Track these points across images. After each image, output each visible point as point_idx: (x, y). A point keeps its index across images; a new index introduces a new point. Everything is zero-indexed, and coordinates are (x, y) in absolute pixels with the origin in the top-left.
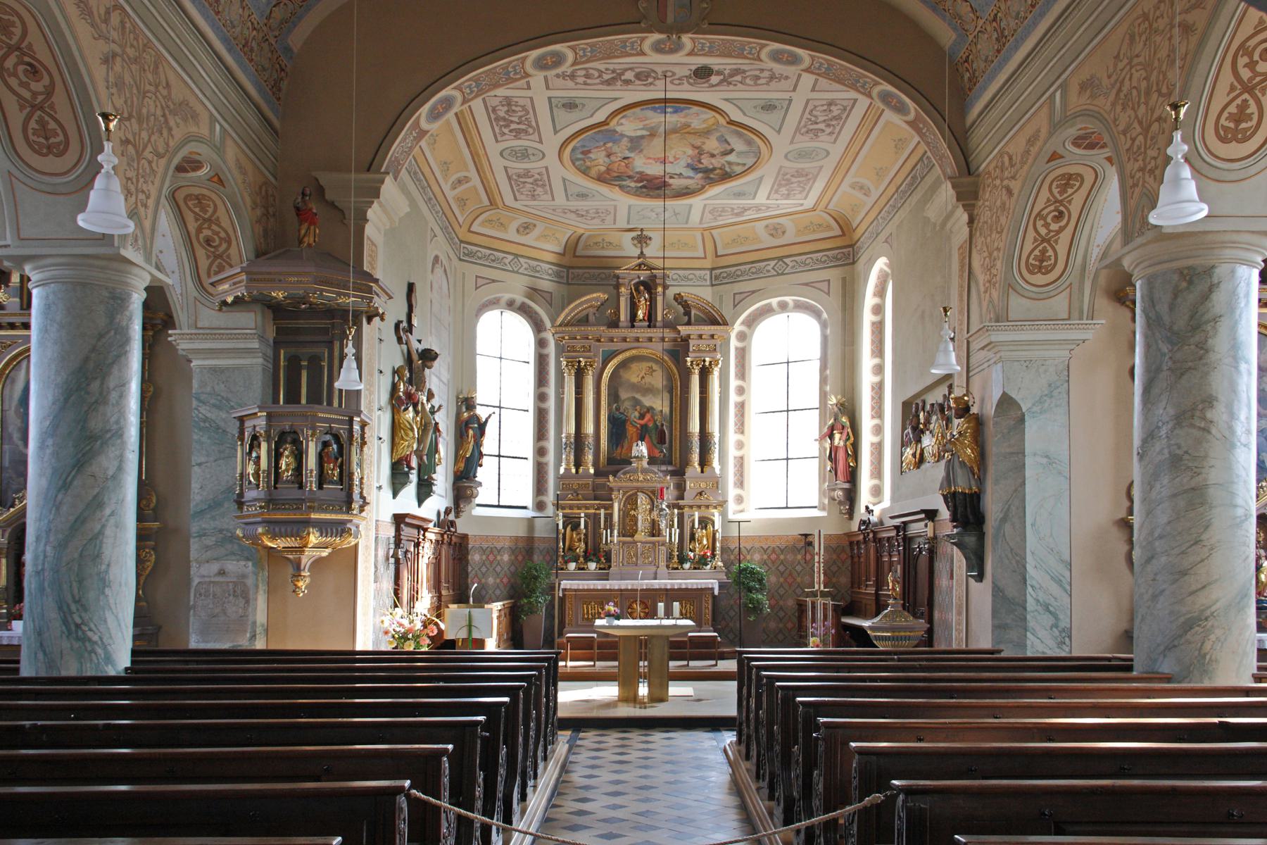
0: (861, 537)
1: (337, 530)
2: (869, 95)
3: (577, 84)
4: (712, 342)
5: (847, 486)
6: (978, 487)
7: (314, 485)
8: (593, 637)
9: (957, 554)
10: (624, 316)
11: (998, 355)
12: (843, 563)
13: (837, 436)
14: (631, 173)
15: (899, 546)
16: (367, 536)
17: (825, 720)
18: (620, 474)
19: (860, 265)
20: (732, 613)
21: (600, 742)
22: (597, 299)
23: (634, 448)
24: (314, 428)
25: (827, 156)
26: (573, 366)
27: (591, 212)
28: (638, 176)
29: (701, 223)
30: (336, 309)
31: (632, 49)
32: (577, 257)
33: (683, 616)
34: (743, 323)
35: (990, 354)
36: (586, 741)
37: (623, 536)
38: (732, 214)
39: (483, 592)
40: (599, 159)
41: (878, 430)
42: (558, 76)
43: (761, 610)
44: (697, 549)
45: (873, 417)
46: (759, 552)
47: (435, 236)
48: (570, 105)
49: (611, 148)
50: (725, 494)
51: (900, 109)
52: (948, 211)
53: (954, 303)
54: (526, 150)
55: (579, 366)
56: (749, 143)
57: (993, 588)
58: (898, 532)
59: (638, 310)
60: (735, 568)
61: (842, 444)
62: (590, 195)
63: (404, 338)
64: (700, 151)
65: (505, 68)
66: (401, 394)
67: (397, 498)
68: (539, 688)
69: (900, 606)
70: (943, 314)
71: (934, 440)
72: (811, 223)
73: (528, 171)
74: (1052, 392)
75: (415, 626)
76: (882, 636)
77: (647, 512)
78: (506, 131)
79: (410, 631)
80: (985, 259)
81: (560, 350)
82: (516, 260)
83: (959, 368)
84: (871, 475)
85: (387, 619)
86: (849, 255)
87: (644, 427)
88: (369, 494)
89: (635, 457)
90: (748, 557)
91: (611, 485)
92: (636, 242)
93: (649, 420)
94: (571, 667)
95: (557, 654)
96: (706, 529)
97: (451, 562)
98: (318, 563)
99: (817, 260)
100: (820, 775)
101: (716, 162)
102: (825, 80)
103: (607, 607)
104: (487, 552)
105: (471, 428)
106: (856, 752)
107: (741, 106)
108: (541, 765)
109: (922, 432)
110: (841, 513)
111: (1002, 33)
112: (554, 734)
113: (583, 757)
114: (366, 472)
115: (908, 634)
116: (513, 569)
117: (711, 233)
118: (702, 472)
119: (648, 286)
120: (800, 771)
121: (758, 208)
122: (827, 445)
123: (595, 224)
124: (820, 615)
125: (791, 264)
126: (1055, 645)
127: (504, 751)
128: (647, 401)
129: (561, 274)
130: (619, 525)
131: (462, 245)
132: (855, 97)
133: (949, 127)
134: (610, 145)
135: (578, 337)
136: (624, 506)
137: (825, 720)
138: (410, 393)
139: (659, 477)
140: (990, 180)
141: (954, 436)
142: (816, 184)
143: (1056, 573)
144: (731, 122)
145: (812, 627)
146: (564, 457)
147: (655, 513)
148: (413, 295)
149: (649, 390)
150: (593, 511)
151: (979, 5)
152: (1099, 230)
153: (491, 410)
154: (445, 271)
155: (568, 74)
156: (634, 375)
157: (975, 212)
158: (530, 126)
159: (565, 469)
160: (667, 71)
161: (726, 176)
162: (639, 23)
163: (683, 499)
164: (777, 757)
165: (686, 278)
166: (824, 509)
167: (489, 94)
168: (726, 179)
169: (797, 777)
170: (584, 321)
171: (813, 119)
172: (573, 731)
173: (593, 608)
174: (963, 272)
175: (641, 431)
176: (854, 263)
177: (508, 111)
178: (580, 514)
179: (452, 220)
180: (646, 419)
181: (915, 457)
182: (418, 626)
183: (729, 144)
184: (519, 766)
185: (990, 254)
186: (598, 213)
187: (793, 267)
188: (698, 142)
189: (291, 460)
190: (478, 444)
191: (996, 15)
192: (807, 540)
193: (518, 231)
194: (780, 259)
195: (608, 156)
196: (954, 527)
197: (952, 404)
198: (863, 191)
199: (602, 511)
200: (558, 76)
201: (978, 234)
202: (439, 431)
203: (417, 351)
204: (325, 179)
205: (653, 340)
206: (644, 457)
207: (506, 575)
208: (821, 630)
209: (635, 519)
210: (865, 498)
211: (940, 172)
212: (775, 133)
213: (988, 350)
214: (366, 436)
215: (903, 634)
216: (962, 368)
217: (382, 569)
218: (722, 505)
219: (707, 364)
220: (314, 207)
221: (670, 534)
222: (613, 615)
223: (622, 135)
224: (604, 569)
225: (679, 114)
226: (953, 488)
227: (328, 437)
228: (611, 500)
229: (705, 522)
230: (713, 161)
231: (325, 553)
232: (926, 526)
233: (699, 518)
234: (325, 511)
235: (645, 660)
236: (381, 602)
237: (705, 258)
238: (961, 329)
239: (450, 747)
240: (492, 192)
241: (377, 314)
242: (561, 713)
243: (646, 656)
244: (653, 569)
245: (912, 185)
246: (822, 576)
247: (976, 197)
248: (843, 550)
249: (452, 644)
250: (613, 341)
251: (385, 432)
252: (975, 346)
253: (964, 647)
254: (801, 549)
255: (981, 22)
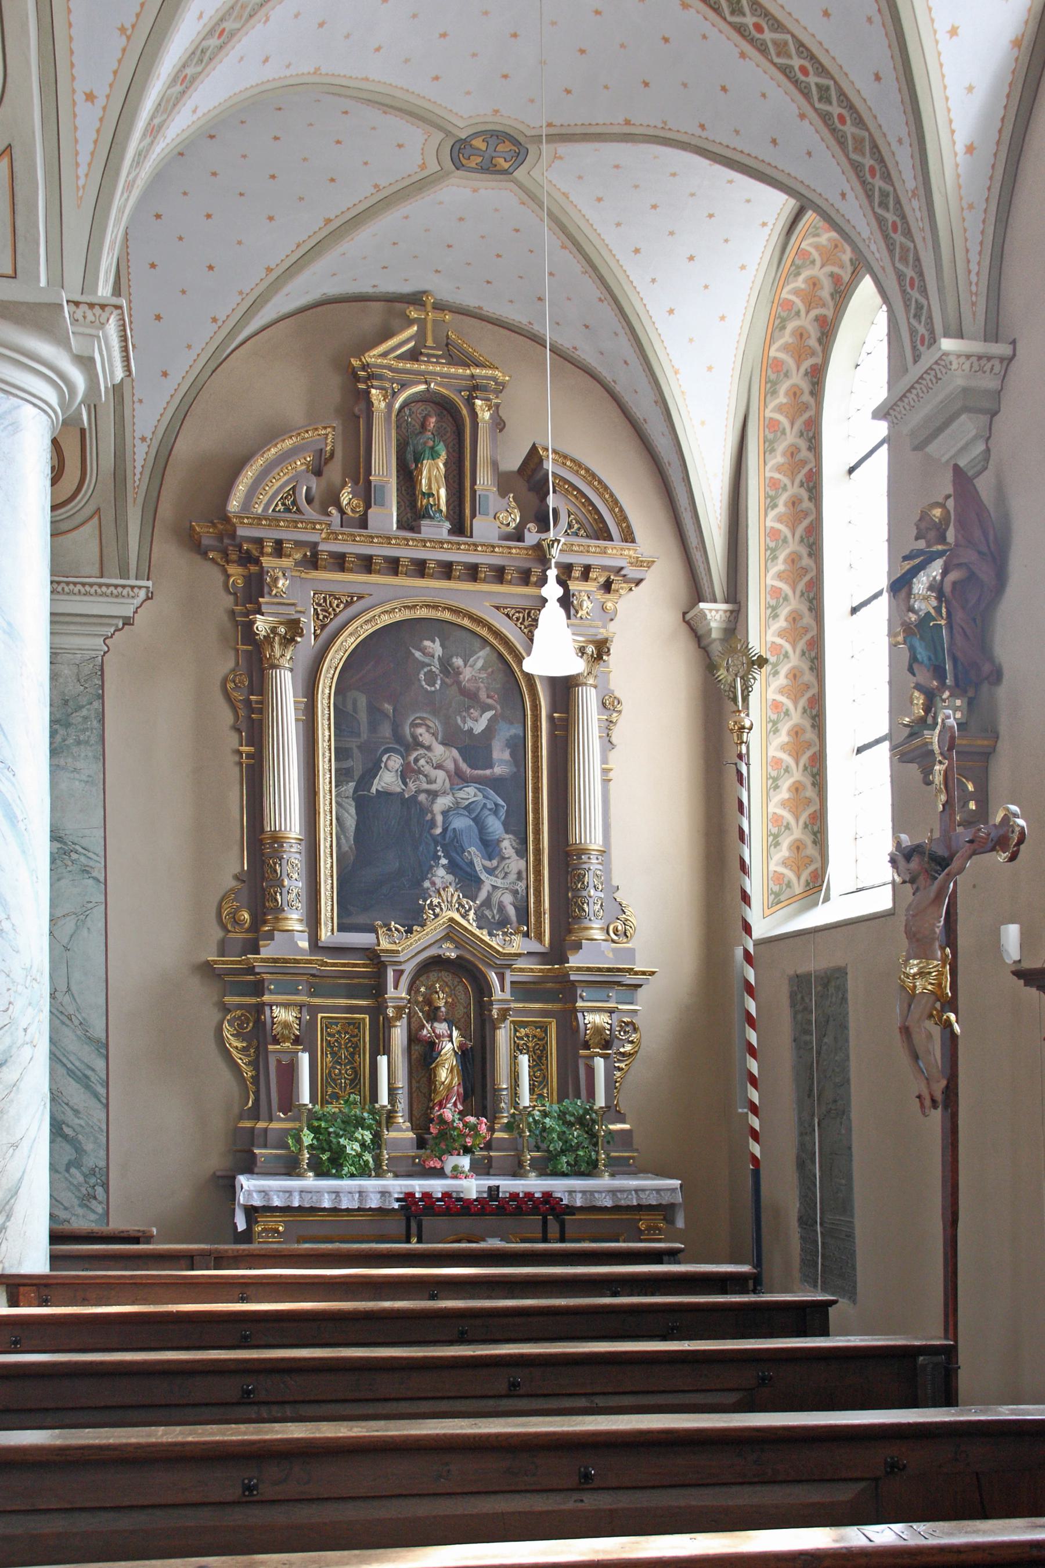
74: (68, 715)
126: (76, 1202)
143: (77, 1064)
152: (137, 405)
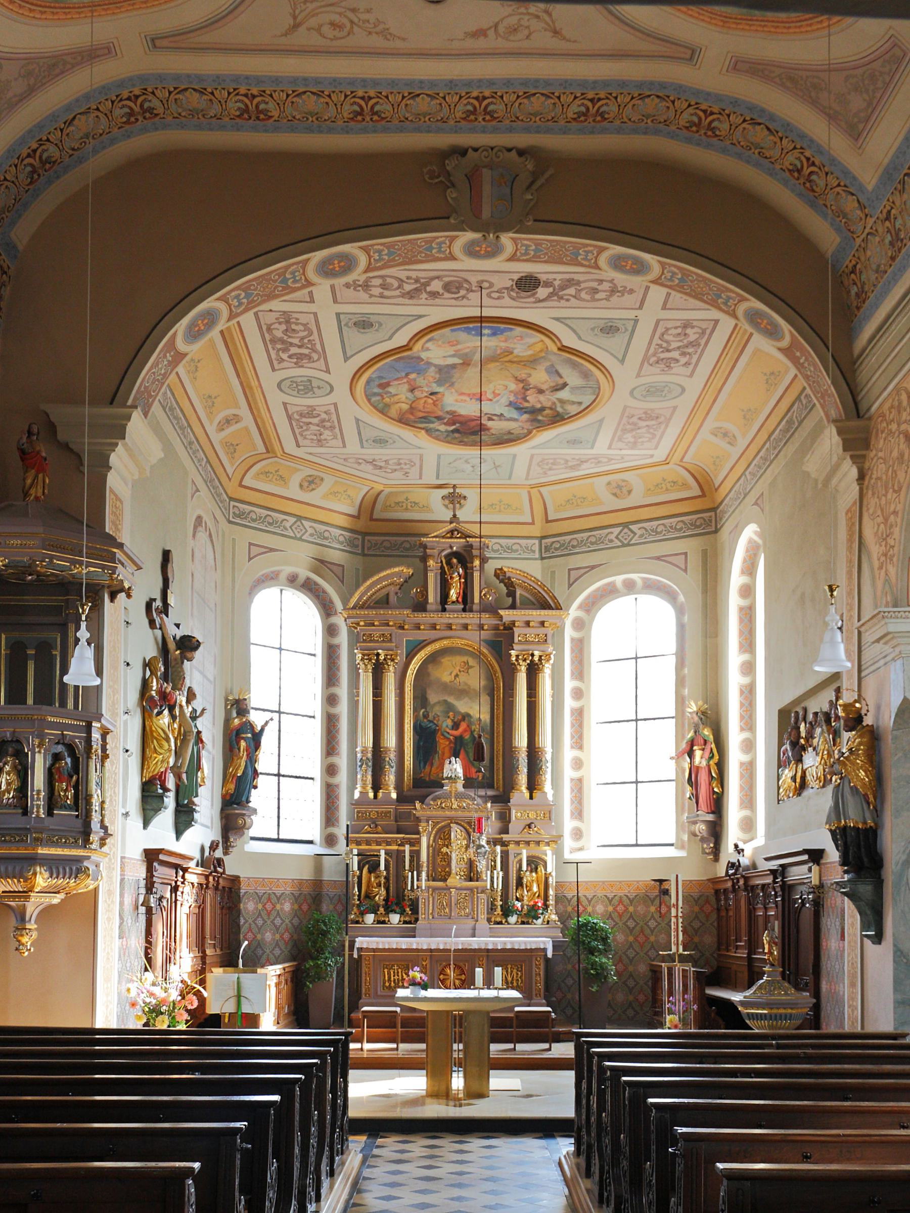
0: (729, 884)
1: (71, 869)
2: (735, 316)
3: (371, 296)
4: (542, 631)
5: (711, 817)
6: (874, 821)
7: (42, 811)
8: (396, 1012)
9: (849, 907)
10: (433, 596)
11: (897, 650)
12: (707, 916)
13: (698, 753)
14: (440, 413)
15: (776, 896)
16: (110, 878)
17: (685, 1130)
18: (429, 800)
19: (725, 533)
20: (570, 982)
21: (402, 1152)
22: (399, 575)
23: (447, 767)
24: (41, 737)
25: (681, 394)
26: (370, 660)
27: (391, 462)
28: (448, 416)
29: (527, 479)
30: (70, 582)
31: (439, 251)
32: (377, 520)
33: (508, 985)
34: (580, 607)
35: (887, 649)
36: (384, 1150)
37: (434, 880)
38: (566, 468)
39: (260, 952)
40: (400, 393)
41: (749, 746)
42: (347, 286)
43: (606, 977)
44: (525, 898)
45: (742, 729)
46: (603, 902)
47: (198, 490)
48: (364, 324)
49: (415, 380)
50: (560, 825)
51: (772, 332)
52: (833, 463)
53: (841, 580)
54: (310, 381)
55: (378, 659)
56: (586, 375)
57: (895, 953)
58: (775, 878)
59: (450, 589)
60: (573, 923)
61: (704, 763)
62: (391, 441)
63: (158, 621)
64: (525, 385)
65: (282, 273)
66: (154, 693)
67: (150, 828)
68: (322, 1082)
69: (778, 973)
70: (829, 594)
71: (819, 759)
72: (664, 480)
73: (312, 408)
75: (169, 996)
76: (757, 1014)
77: (463, 850)
78: (284, 356)
79: (163, 1002)
80: (879, 525)
81: (354, 639)
82: (299, 523)
83: (849, 664)
84: (741, 804)
85: (133, 987)
86: (710, 521)
87: (459, 740)
88: (113, 823)
89: (447, 778)
90: (590, 909)
91: (418, 814)
92: (447, 502)
93: (465, 731)
94: (368, 1051)
95: (347, 1035)
96: (536, 872)
97: (218, 911)
98: (47, 912)
99: (671, 527)
100: (678, 1204)
101: (545, 400)
102: (679, 295)
103: (411, 973)
104: (264, 899)
105: (243, 738)
106: (724, 1176)
107: (575, 327)
108: (326, 1183)
109: (804, 749)
110: (704, 852)
111: (897, 235)
112: (343, 1141)
113: (379, 1172)
114: (108, 794)
115: (790, 1011)
116: (296, 921)
117: (540, 492)
118: (531, 798)
119: (463, 558)
120: (653, 1196)
121: (597, 460)
122: (687, 766)
123: (396, 479)
124: (678, 985)
125: (639, 532)
127: (273, 1166)
128: (463, 706)
129: (356, 543)
130: (428, 867)
131: (232, 503)
132: (716, 318)
133: (833, 356)
134: (413, 376)
135: (376, 623)
136: (434, 841)
137: (685, 1130)
138: (165, 692)
139: (477, 805)
140: (884, 424)
141: (843, 754)
142: (669, 430)
144: (563, 349)
145: (669, 1002)
146: (359, 776)
147: (472, 850)
148: (169, 566)
149: (463, 692)
150: (396, 847)
151: (868, 199)
153: (268, 715)
154: (210, 535)
155: (360, 283)
156: (446, 672)
157: (867, 465)
158: (315, 351)
159: (361, 792)
160: (483, 281)
161: (558, 419)
162: (448, 218)
163: (508, 833)
164: (624, 1176)
165: (509, 549)
166: (682, 847)
167: (260, 308)
168: (558, 421)
169: (650, 1204)
170: (384, 602)
171: (665, 345)
172: (369, 1136)
173: (395, 974)
174: (852, 543)
175: (455, 744)
176: (716, 531)
177: (287, 330)
178: (379, 851)
179: (220, 471)
180: (461, 729)
181: (795, 781)
182: (174, 995)
183: (561, 377)
184: (295, 1185)
185: (886, 520)
186: (400, 464)
187: (641, 536)
188: (522, 373)
189: (13, 777)
190: (252, 760)
191: (889, 212)
192: (661, 887)
193: (301, 486)
194: (625, 525)
195: (412, 390)
196: (846, 872)
197: (841, 713)
198: (727, 439)
199: (407, 848)
200: (347, 286)
201: (870, 492)
202: (202, 741)
203: (174, 638)
204: (58, 413)
205: (470, 627)
206: (457, 777)
207: (287, 930)
208: (680, 1006)
209: (447, 858)
210: (733, 833)
211: (822, 414)
212: (618, 363)
213: (885, 643)
214: (108, 747)
215: (782, 1011)
216: (853, 665)
217: (130, 921)
218: (556, 840)
219: (536, 659)
220: (43, 449)
221: (492, 878)
222: (419, 984)
223: (429, 364)
224: (410, 923)
225: (499, 336)
226: (843, 822)
227: (60, 748)
228: (418, 833)
229: (535, 863)
230: (542, 398)
231: (56, 899)
232: (810, 870)
233: (528, 857)
234: (56, 844)
235: (460, 1042)
236: (128, 965)
237: (533, 523)
238: (851, 616)
239: (197, 1165)
240: (268, 436)
241: (122, 590)
242: (352, 1113)
243: (461, 1037)
244: (471, 923)
245: (788, 431)
246: (681, 934)
247: (866, 444)
248: (707, 901)
249: (216, 1020)
250: (419, 629)
251: (133, 742)
252: (868, 638)
253: (859, 1029)
254: (654, 899)
255: (870, 221)
